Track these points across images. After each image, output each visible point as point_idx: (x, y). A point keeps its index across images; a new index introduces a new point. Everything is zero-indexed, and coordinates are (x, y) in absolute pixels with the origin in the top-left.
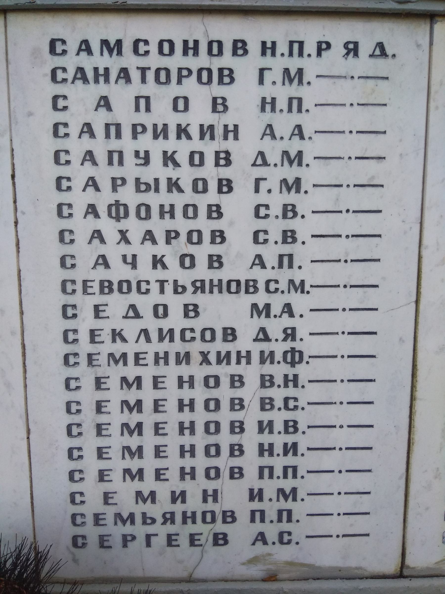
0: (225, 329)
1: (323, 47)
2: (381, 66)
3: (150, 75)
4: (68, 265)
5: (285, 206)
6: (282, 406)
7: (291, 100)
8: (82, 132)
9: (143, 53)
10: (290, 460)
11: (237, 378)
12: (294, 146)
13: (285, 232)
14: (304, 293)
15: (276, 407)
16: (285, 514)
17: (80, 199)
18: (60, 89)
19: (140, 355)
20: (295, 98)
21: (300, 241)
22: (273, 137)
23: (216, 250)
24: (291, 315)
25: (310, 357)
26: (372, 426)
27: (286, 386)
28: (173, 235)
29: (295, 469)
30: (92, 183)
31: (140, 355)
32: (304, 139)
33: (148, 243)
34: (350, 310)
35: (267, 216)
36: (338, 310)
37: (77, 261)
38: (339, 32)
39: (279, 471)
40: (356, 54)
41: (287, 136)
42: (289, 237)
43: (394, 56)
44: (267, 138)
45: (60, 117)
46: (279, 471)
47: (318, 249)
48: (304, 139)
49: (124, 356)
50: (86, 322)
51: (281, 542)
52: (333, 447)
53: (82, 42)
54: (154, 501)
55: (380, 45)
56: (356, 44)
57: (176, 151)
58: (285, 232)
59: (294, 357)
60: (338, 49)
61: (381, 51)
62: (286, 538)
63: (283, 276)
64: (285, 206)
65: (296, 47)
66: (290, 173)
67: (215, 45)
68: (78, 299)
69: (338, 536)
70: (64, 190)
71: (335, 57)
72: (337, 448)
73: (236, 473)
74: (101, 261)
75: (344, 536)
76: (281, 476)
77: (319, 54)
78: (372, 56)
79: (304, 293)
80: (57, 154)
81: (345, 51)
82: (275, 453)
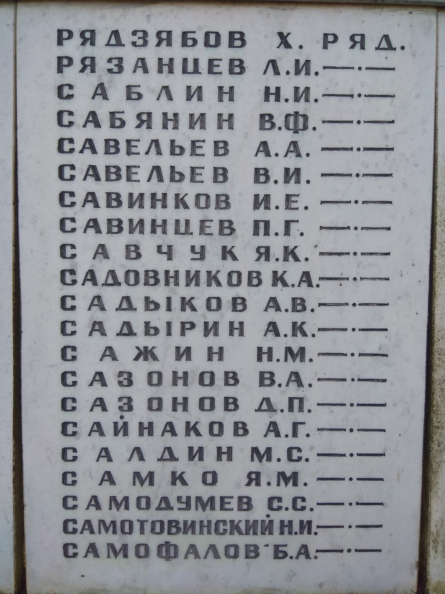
0: (232, 34)
1: (329, 40)
3: (148, 527)
4: (69, 408)
8: (87, 121)
10: (302, 81)
12: (296, 343)
13: (294, 299)
17: (84, 417)
18: (68, 238)
19: (197, 170)
21: (309, 308)
22: (308, 557)
23: (221, 162)
24: (300, 384)
25: (317, 551)
30: (100, 403)
31: (197, 170)
36: (352, 122)
37: (79, 353)
38: (346, 21)
40: (363, 48)
41: (282, 153)
42: (298, 329)
45: (66, 105)
47: (324, 417)
48: (312, 286)
49: (125, 547)
50: (81, 105)
52: (350, 147)
53: (95, 297)
54: (151, 483)
55: (386, 37)
57: (184, 472)
58: (294, 299)
59: (302, 67)
60: (344, 42)
61: (387, 44)
68: (76, 238)
70: (69, 435)
71: (341, 52)
72: (352, 228)
74: (103, 454)
75: (365, 149)
76: (290, 433)
80: (63, 299)
81: (352, 43)
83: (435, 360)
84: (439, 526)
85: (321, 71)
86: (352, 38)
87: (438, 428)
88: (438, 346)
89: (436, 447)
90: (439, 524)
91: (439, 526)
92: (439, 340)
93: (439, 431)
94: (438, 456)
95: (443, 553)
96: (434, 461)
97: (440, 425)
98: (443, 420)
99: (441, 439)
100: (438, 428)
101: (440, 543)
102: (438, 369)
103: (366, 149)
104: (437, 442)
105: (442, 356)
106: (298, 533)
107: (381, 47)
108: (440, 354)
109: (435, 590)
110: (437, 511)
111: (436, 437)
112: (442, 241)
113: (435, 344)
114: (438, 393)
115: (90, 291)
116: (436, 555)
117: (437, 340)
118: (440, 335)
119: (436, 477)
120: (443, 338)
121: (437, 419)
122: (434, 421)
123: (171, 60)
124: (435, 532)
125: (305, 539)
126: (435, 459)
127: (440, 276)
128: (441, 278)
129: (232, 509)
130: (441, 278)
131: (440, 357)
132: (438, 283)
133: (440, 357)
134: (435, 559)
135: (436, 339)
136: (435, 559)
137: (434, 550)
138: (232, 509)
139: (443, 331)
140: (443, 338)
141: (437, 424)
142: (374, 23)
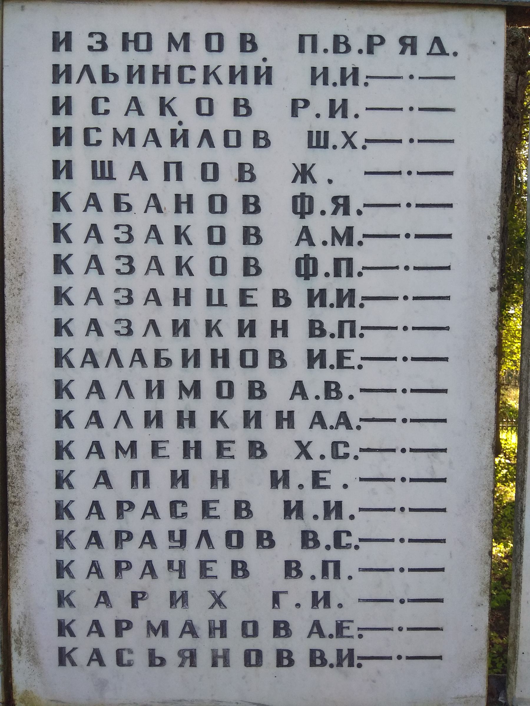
1: (373, 43)
2: (439, 65)
5: (328, 384)
6: (331, 543)
7: (341, 324)
9: (103, 112)
11: (285, 654)
14: (353, 666)
15: (323, 545)
16: (344, 264)
20: (343, 259)
21: (345, 395)
26: (448, 298)
27: (343, 83)
28: (125, 536)
29: (353, 323)
32: (352, 429)
33: (95, 457)
34: (418, 206)
35: (346, 455)
38: (392, 23)
39: (331, 297)
40: (414, 52)
43: (455, 54)
44: (298, 398)
46: (331, 297)
48: (352, 429)
51: (335, 455)
55: (437, 40)
56: (414, 38)
60: (393, 45)
62: (342, 450)
63: (331, 411)
64: (328, 384)
65: (347, 326)
66: (341, 223)
67: (225, 386)
69: (402, 570)
71: (388, 59)
73: (277, 359)
77: (370, 51)
78: (429, 54)
79: (353, 666)
82: (331, 81)
83: (8, 421)
84: (21, 623)
85: (355, 573)
86: (402, 40)
87: (14, 503)
88: (11, 405)
89: (13, 526)
90: (21, 620)
91: (21, 623)
92: (12, 398)
93: (17, 507)
94: (16, 538)
95: (28, 656)
96: (12, 544)
97: (16, 500)
98: (20, 495)
99: (18, 518)
100: (14, 503)
101: (24, 643)
102: (13, 433)
103: (412, 421)
104: (13, 522)
105: (16, 417)
106: (335, 635)
107: (433, 52)
108: (13, 414)
109: (23, 701)
110: (18, 604)
111: (12, 514)
112: (11, 277)
113: (8, 403)
114: (13, 462)
115: (89, 374)
116: (20, 658)
117: (9, 397)
118: (14, 391)
119: (14, 563)
120: (17, 395)
121: (13, 492)
122: (10, 496)
123: (326, 69)
124: (17, 630)
125: (346, 313)
126: (12, 542)
127: (11, 320)
128: (13, 322)
129: (352, 637)
130: (13, 322)
131: (14, 417)
132: (9, 328)
133: (14, 417)
134: (19, 663)
135: (8, 396)
136: (19, 663)
137: (17, 651)
138: (352, 637)
139: (16, 387)
140: (17, 395)
141: (13, 499)
142: (423, 24)
